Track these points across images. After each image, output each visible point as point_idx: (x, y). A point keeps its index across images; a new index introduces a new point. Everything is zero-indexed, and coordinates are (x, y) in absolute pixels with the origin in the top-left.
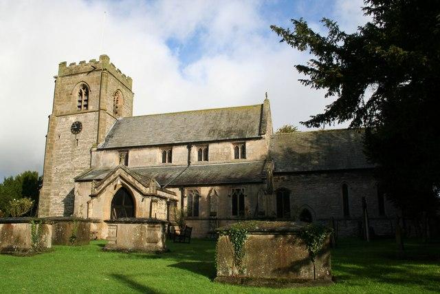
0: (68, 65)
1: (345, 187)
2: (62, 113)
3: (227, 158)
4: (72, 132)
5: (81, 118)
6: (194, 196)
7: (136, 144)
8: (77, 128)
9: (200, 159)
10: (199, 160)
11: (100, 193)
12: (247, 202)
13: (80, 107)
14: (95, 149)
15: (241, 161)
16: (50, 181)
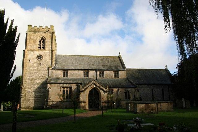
0: (33, 27)
1: (152, 90)
2: (31, 49)
3: (112, 77)
4: (39, 60)
5: (42, 53)
6: (65, 90)
7: (73, 68)
8: (40, 58)
9: (100, 77)
10: (63, 77)
11: (85, 90)
12: (130, 94)
13: (40, 48)
14: (51, 68)
15: (65, 78)
16: (26, 82)
